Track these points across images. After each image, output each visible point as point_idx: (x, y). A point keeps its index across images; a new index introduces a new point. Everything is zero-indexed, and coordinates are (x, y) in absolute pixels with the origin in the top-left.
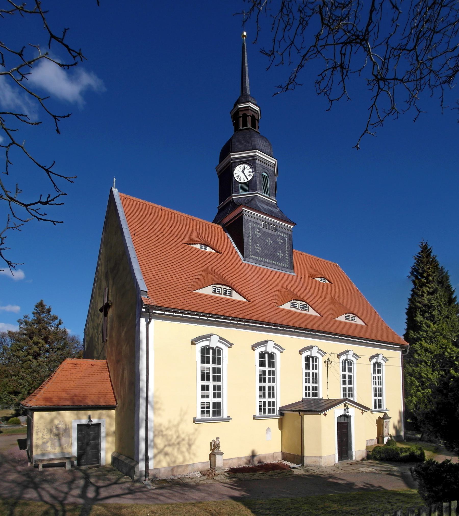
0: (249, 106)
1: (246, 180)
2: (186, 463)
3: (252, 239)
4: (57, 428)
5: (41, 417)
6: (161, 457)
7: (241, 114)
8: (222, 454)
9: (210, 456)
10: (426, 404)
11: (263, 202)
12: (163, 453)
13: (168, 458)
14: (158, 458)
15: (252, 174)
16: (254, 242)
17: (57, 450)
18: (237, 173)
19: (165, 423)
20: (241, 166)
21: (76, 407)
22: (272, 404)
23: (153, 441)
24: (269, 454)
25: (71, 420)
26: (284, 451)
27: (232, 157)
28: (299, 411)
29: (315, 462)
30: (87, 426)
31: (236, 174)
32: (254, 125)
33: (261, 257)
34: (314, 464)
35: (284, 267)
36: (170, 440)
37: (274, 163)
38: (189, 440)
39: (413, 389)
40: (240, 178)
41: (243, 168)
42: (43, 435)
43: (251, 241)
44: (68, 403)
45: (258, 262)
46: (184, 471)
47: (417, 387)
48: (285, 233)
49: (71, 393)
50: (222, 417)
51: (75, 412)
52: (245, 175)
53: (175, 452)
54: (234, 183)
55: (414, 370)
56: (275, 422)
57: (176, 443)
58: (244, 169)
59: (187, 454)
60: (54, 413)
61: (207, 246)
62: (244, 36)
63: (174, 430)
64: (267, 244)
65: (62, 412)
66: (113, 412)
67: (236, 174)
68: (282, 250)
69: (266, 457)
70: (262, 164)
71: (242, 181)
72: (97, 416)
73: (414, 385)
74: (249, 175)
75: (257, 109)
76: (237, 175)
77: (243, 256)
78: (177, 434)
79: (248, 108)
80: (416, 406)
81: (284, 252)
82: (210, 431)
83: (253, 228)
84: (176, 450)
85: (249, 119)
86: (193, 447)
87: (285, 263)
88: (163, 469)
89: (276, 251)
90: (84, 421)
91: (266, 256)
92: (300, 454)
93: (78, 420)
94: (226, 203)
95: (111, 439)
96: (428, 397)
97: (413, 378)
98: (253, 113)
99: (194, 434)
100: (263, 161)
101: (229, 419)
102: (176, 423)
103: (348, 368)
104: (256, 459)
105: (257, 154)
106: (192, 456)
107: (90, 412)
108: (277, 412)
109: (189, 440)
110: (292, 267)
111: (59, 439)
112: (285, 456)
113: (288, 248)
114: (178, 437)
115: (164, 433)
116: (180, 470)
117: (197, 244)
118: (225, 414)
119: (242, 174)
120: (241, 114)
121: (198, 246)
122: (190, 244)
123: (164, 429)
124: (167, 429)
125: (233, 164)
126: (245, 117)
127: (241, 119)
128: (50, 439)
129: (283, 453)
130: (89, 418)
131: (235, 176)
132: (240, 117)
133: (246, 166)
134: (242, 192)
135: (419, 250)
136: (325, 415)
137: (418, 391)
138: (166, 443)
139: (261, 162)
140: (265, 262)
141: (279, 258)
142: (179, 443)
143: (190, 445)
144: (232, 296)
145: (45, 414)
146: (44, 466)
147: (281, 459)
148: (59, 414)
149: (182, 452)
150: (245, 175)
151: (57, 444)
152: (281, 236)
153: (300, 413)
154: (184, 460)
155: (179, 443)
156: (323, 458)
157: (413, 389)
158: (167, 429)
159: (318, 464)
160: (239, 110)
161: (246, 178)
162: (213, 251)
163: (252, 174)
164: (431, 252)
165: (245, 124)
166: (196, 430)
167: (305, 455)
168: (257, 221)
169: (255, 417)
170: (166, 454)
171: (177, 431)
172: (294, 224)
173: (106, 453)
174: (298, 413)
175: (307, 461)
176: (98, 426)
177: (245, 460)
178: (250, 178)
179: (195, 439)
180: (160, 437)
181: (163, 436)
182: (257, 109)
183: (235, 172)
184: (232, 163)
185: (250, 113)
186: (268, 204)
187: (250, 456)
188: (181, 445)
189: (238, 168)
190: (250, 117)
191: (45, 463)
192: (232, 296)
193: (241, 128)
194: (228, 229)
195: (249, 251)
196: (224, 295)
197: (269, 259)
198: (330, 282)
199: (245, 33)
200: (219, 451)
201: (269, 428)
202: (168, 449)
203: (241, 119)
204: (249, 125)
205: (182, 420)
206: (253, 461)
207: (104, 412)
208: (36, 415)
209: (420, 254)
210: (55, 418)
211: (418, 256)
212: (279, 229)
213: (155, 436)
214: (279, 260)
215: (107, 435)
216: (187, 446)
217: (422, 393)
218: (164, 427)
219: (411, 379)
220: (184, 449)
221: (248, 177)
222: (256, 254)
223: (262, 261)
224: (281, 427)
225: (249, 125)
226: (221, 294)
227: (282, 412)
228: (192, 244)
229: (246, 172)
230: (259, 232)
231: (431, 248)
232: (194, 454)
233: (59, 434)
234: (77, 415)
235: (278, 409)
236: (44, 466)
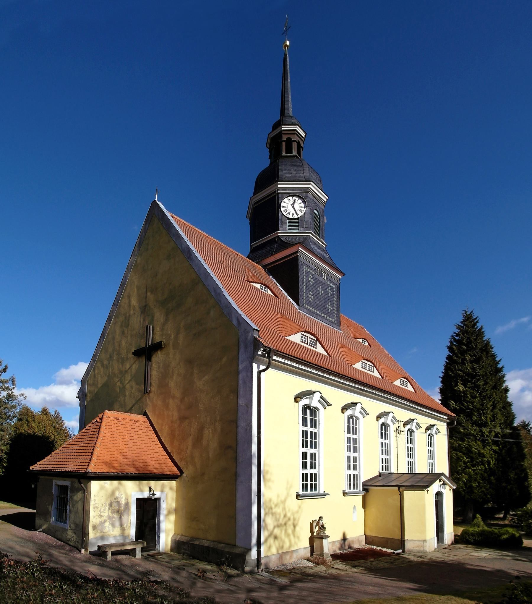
0: (296, 130)
1: (296, 217)
2: (292, 549)
3: (306, 285)
4: (119, 503)
5: (102, 488)
6: (271, 541)
7: (284, 138)
8: (328, 537)
9: (311, 540)
10: (479, 483)
11: (315, 243)
12: (273, 536)
13: (277, 543)
14: (268, 543)
15: (304, 210)
16: (308, 290)
17: (117, 531)
18: (285, 207)
19: (275, 500)
20: (291, 198)
21: (141, 476)
22: (355, 477)
23: (264, 521)
24: (355, 538)
25: (132, 491)
26: (369, 534)
27: (279, 186)
28: (399, 487)
29: (418, 547)
30: (148, 500)
31: (283, 207)
32: (299, 152)
33: (313, 308)
34: (418, 549)
35: (332, 322)
36: (279, 520)
37: (325, 200)
38: (294, 519)
39: (461, 466)
40: (289, 213)
41: (292, 201)
42: (100, 511)
43: (305, 287)
44: (131, 470)
45: (310, 313)
46: (291, 557)
47: (465, 463)
48: (334, 284)
49: (129, 457)
50: (317, 492)
51: (137, 482)
52: (295, 210)
53: (283, 535)
54: (280, 218)
55: (459, 445)
56: (358, 500)
57: (283, 523)
58: (294, 202)
59: (292, 537)
60: (115, 483)
61: (267, 286)
62: (287, 46)
63: (281, 506)
64: (318, 294)
65: (124, 482)
66: (174, 483)
67: (283, 207)
68: (331, 303)
69: (353, 541)
70: (315, 200)
71: (291, 216)
72: (159, 488)
73: (461, 461)
74: (300, 211)
75: (303, 134)
76: (285, 208)
77: (298, 304)
78: (284, 512)
79: (294, 132)
80: (465, 484)
81: (332, 305)
82: (311, 510)
83: (308, 273)
84: (283, 532)
85: (294, 145)
86: (297, 528)
87: (333, 318)
88: (273, 557)
89: (326, 303)
90: (146, 494)
91: (317, 307)
92: (398, 537)
93: (139, 493)
94: (263, 242)
95: (172, 518)
96: (481, 474)
97: (459, 454)
98: (299, 139)
99: (297, 512)
100: (315, 196)
101: (324, 495)
102: (283, 498)
103: (311, 442)
104: (347, 543)
105: (310, 186)
106: (297, 540)
107: (152, 483)
108: (360, 487)
109: (294, 519)
110: (339, 324)
111: (121, 518)
112: (369, 540)
113: (336, 301)
114: (285, 516)
115: (274, 510)
116: (288, 557)
117: (258, 283)
118: (322, 489)
119: (291, 208)
120: (284, 138)
121: (258, 286)
122: (252, 282)
123: (273, 506)
124: (276, 505)
125: (280, 195)
126: (289, 142)
127: (284, 144)
128: (109, 518)
129: (367, 537)
130: (150, 489)
131: (282, 209)
132: (284, 141)
133: (297, 199)
134: (290, 229)
135: (461, 318)
136: (428, 491)
137: (467, 467)
138: (276, 524)
139: (314, 197)
140: (317, 314)
141: (328, 311)
142: (285, 524)
143: (294, 526)
144: (316, 348)
145: (108, 484)
146: (113, 553)
147: (364, 544)
148: (120, 484)
149: (288, 535)
150: (295, 210)
151: (117, 524)
152: (331, 286)
153: (400, 489)
154: (290, 546)
155: (285, 524)
156: (428, 541)
157: (461, 466)
158: (276, 505)
159: (422, 549)
160: (281, 133)
161: (296, 214)
162: (272, 294)
163: (304, 210)
164: (477, 322)
165: (289, 150)
166: (300, 507)
167: (406, 537)
168: (311, 265)
169: (344, 494)
170: (276, 538)
171: (284, 509)
172: (343, 274)
173: (167, 535)
174: (397, 488)
175: (408, 546)
176: (158, 499)
177: (338, 545)
178: (301, 214)
179: (299, 519)
180: (271, 516)
181: (273, 514)
182: (303, 134)
183: (283, 204)
184: (278, 194)
185: (294, 138)
186: (319, 247)
187: (341, 540)
188: (287, 525)
189: (286, 200)
190: (296, 143)
191: (114, 549)
192: (316, 348)
193: (284, 154)
194: (273, 270)
195: (303, 299)
196: (310, 345)
197: (320, 311)
198: (370, 345)
199: (288, 43)
200: (324, 533)
201: (355, 506)
202: (277, 531)
203: (284, 144)
204: (294, 153)
205: (288, 494)
206: (345, 546)
207: (166, 483)
208: (95, 485)
209: (462, 323)
210: (117, 489)
211: (459, 325)
212: (329, 277)
213: (266, 514)
214: (328, 314)
215: (169, 513)
216: (292, 527)
217: (474, 470)
218: (273, 503)
219: (457, 454)
220: (290, 531)
221: (298, 212)
222: (309, 303)
223: (314, 313)
224: (364, 506)
225: (294, 153)
226: (307, 344)
227: (365, 487)
228: (254, 282)
229: (297, 206)
230: (312, 278)
231: (476, 318)
232: (298, 538)
233: (119, 511)
234: (139, 485)
235: (361, 485)
236: (113, 553)
